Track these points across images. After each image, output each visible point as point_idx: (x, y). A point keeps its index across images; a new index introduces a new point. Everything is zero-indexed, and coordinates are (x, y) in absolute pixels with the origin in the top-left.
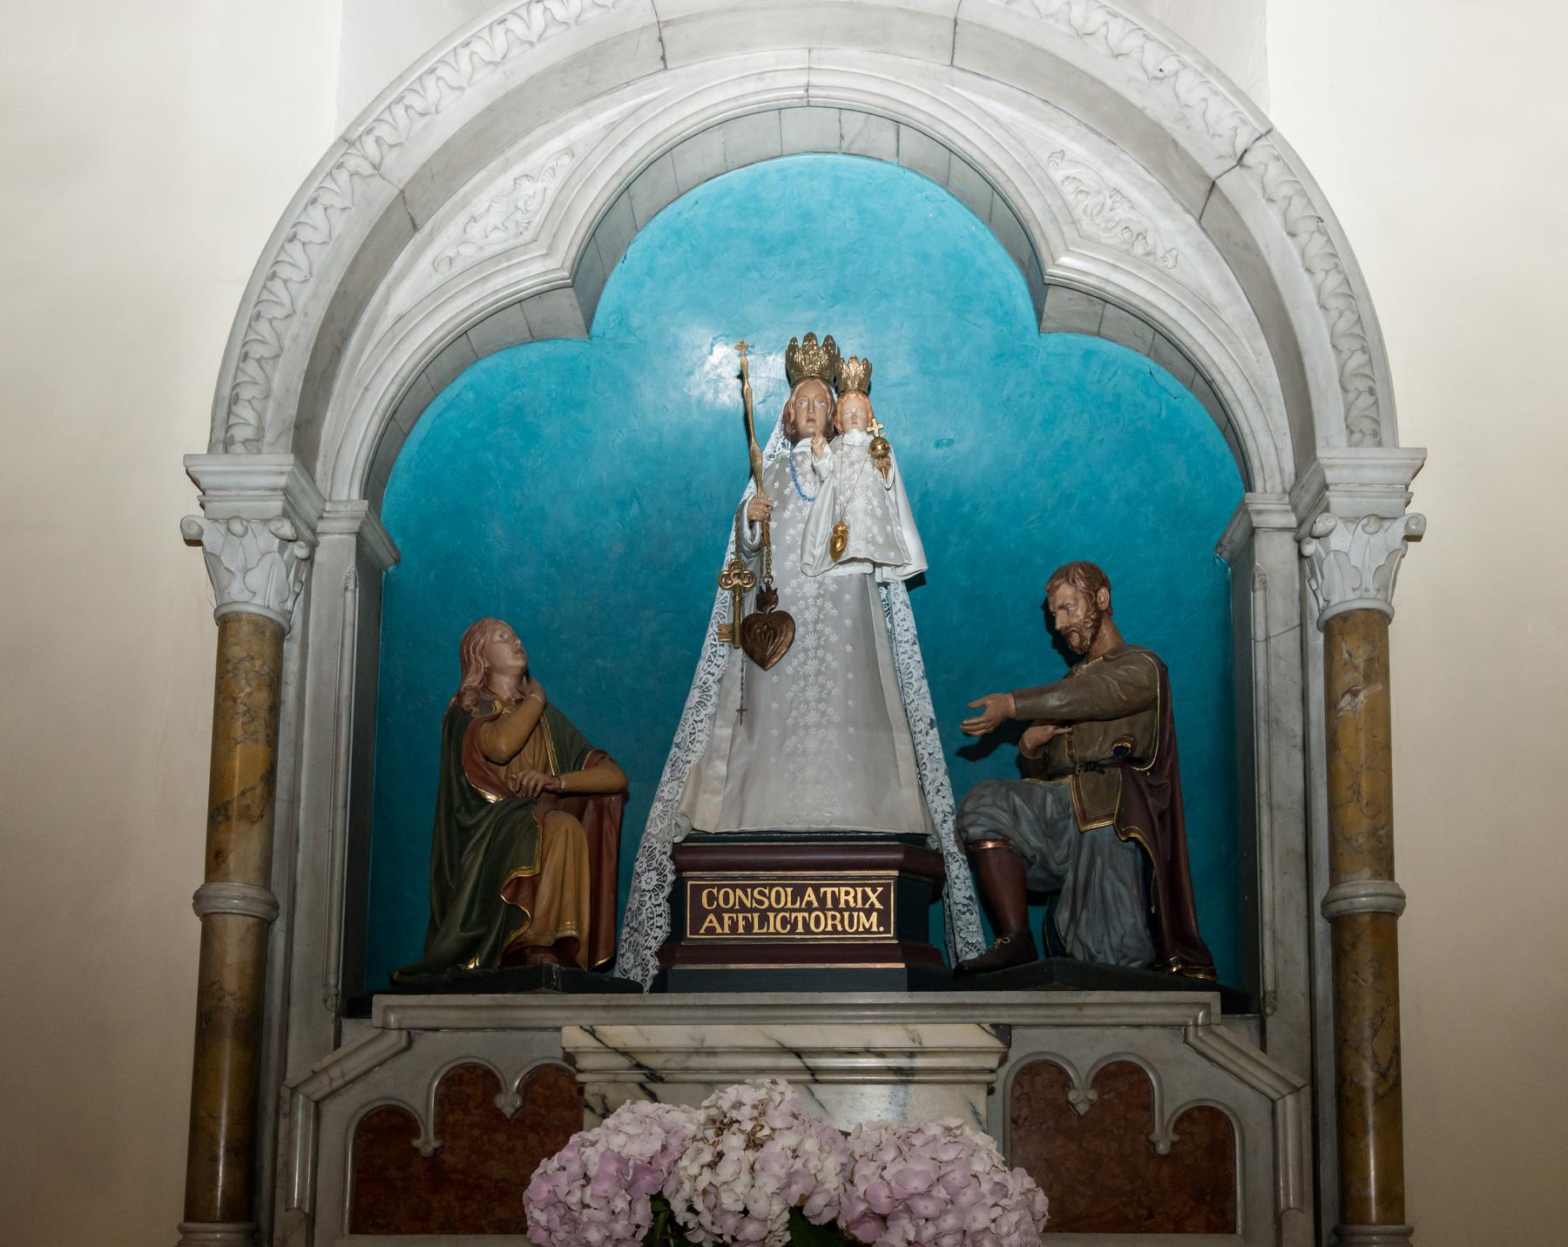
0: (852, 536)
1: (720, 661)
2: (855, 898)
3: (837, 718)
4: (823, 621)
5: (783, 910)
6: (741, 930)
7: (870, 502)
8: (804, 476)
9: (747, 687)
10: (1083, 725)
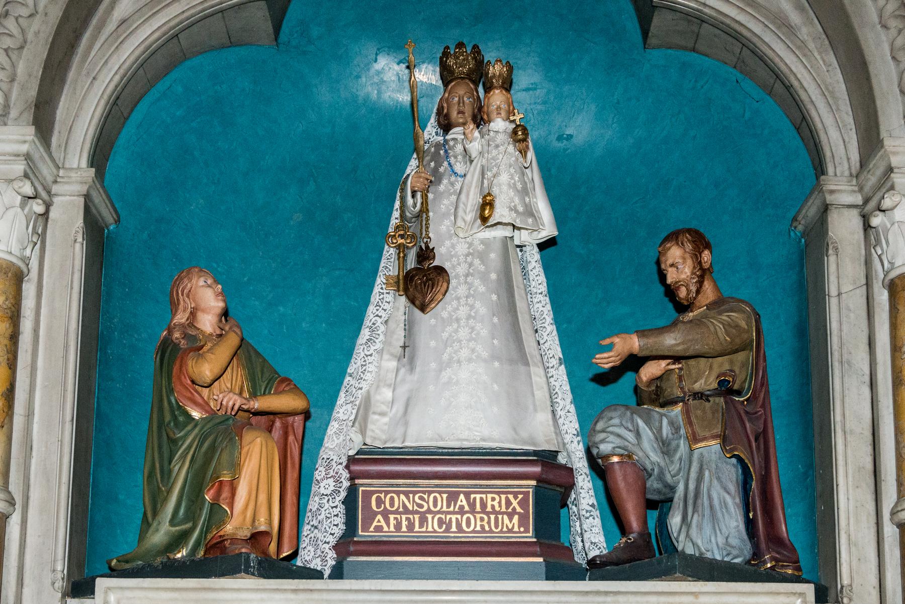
0: (497, 204)
1: (387, 306)
2: (500, 503)
3: (485, 354)
4: (472, 275)
5: (439, 512)
6: (404, 529)
7: (512, 178)
8: (456, 157)
9: (410, 327)
10: (692, 362)
